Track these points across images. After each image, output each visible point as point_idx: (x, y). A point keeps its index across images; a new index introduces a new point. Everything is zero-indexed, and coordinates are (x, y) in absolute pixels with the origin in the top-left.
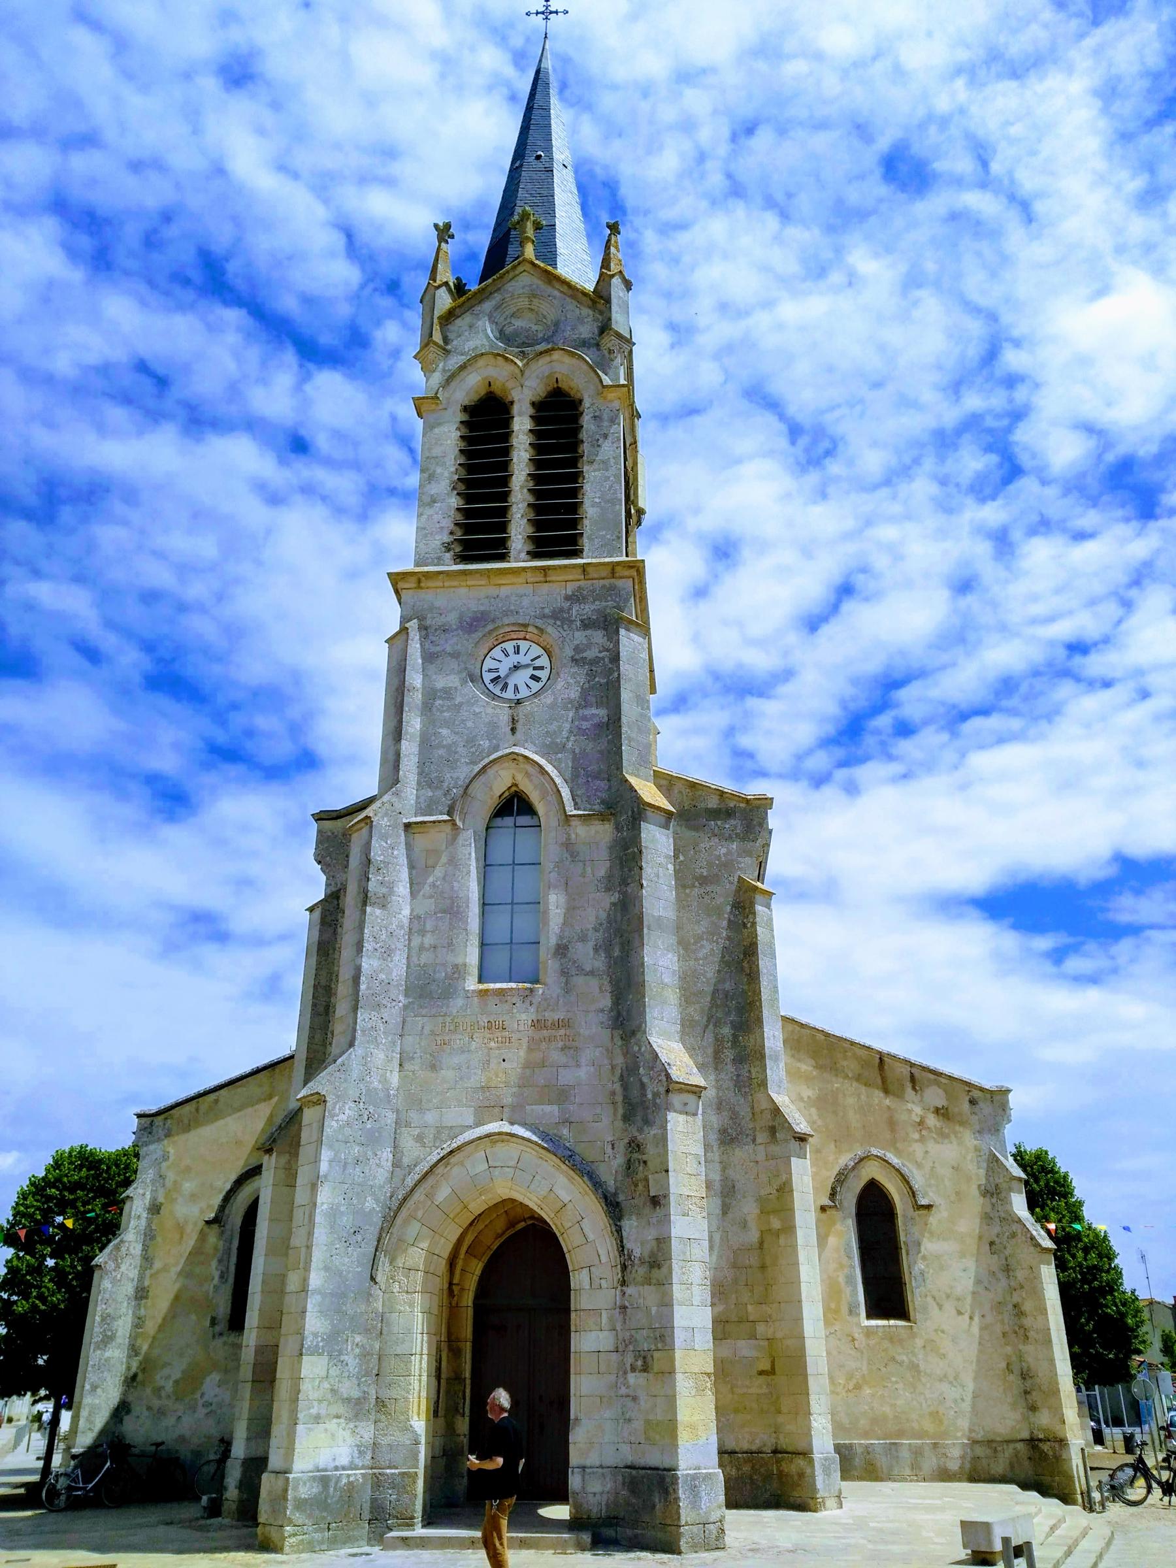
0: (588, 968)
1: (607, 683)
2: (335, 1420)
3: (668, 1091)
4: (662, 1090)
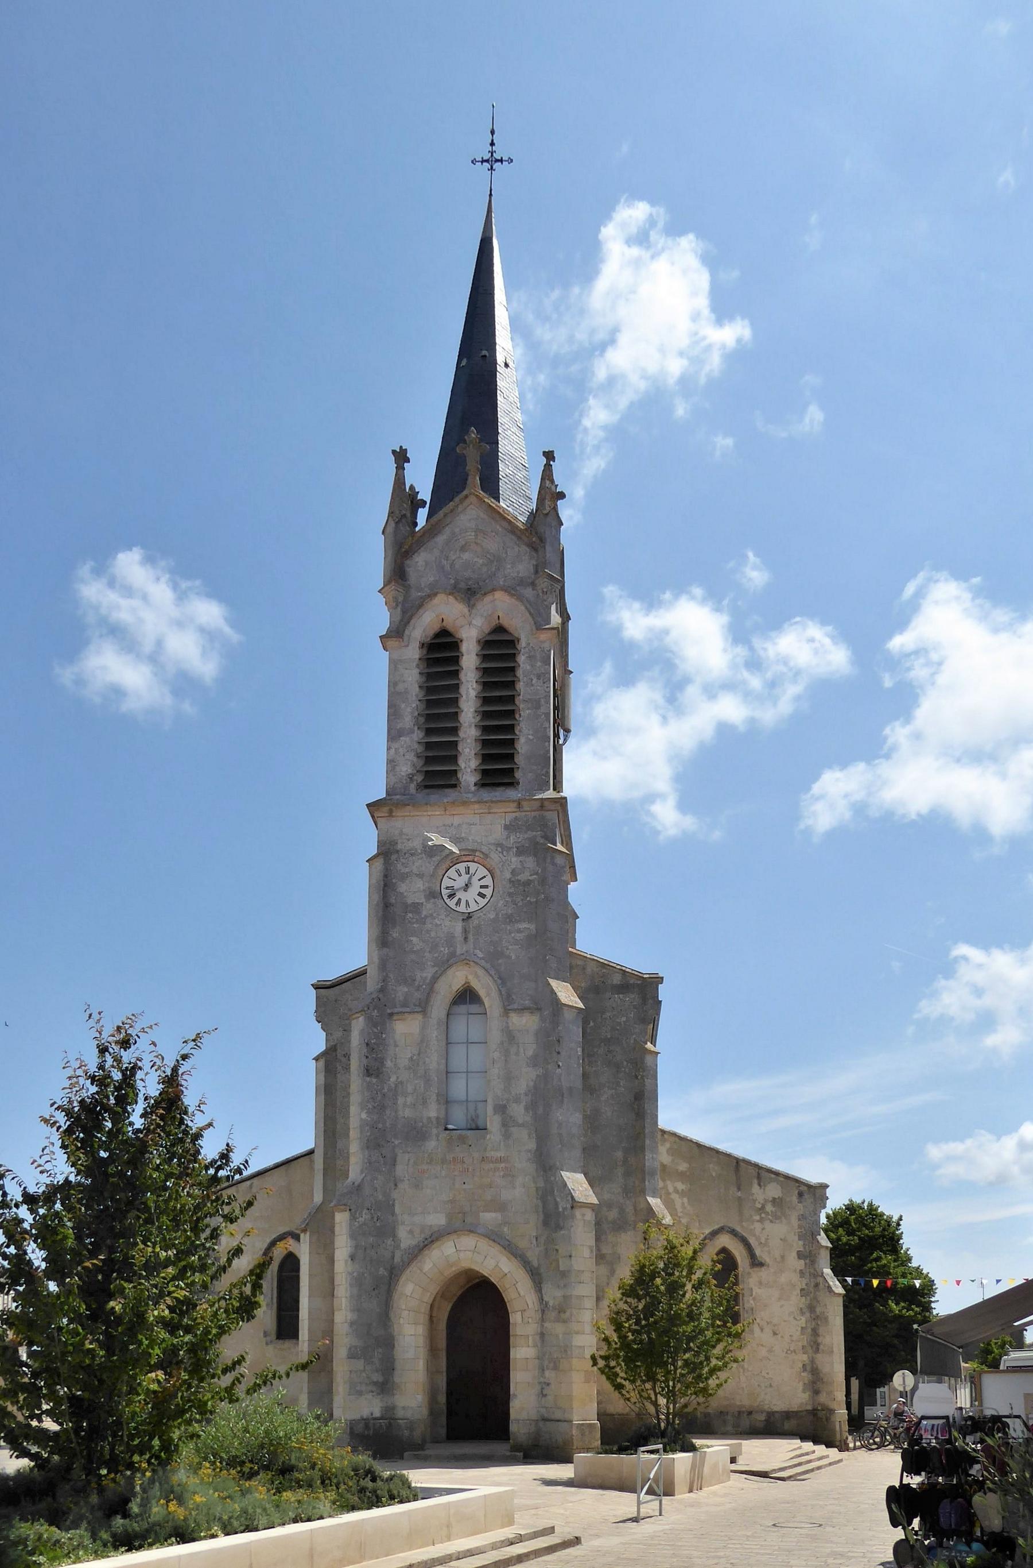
0: (520, 1121)
1: (536, 902)
3: (572, 1207)
4: (569, 1206)
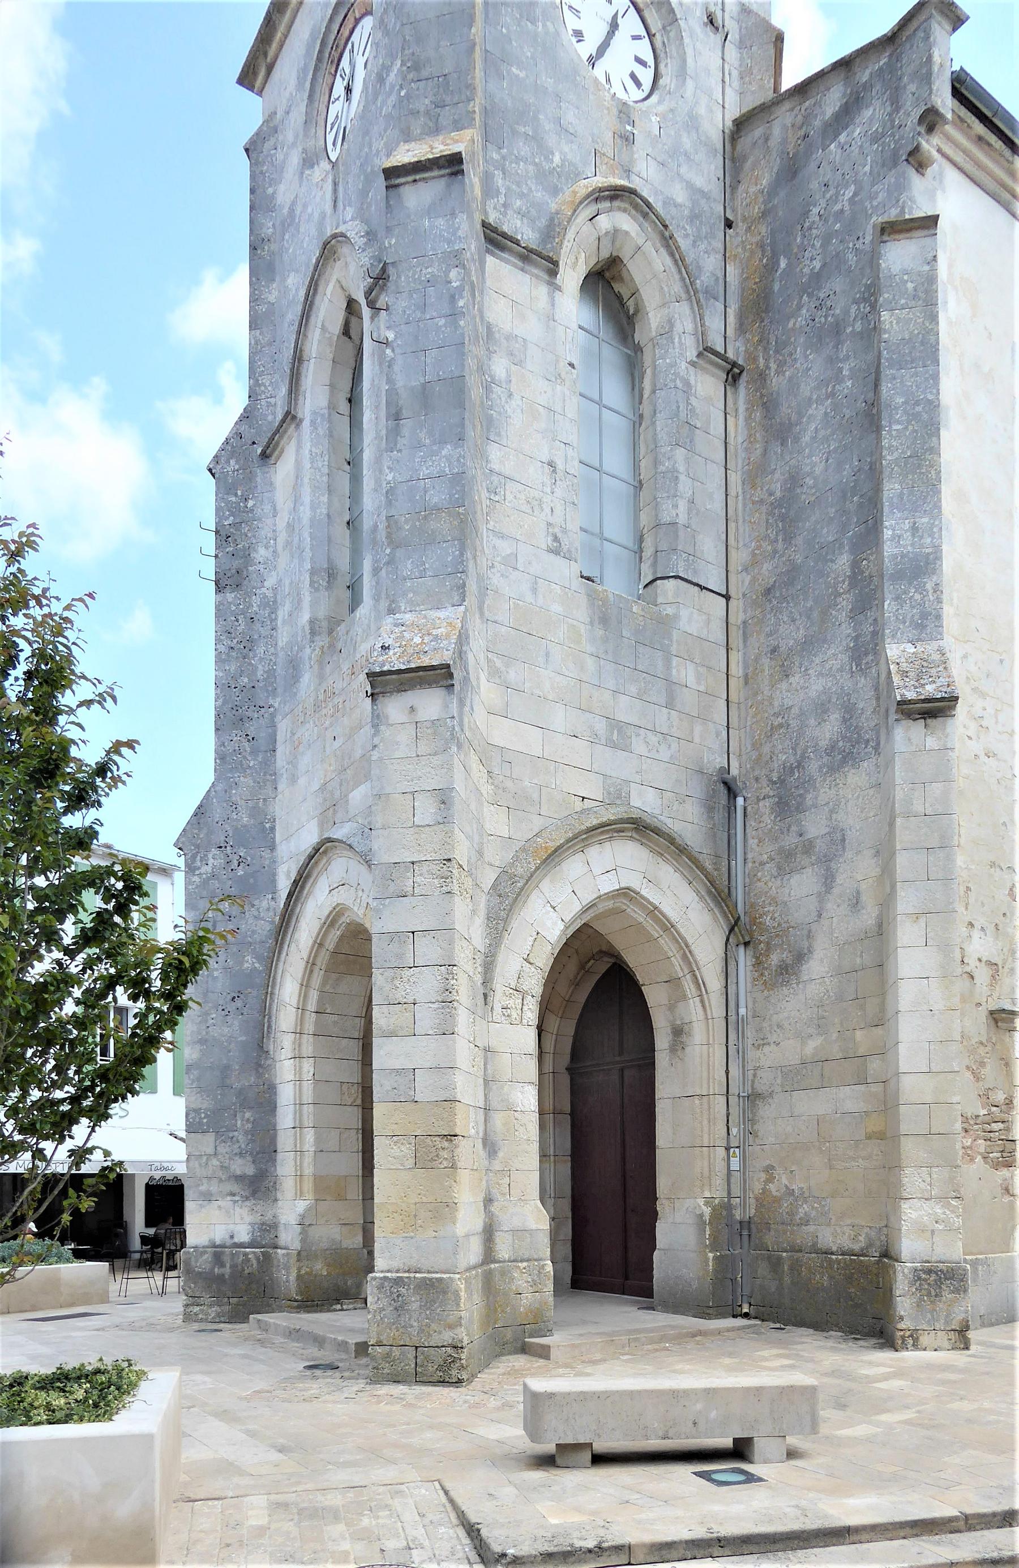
2: (229, 1198)
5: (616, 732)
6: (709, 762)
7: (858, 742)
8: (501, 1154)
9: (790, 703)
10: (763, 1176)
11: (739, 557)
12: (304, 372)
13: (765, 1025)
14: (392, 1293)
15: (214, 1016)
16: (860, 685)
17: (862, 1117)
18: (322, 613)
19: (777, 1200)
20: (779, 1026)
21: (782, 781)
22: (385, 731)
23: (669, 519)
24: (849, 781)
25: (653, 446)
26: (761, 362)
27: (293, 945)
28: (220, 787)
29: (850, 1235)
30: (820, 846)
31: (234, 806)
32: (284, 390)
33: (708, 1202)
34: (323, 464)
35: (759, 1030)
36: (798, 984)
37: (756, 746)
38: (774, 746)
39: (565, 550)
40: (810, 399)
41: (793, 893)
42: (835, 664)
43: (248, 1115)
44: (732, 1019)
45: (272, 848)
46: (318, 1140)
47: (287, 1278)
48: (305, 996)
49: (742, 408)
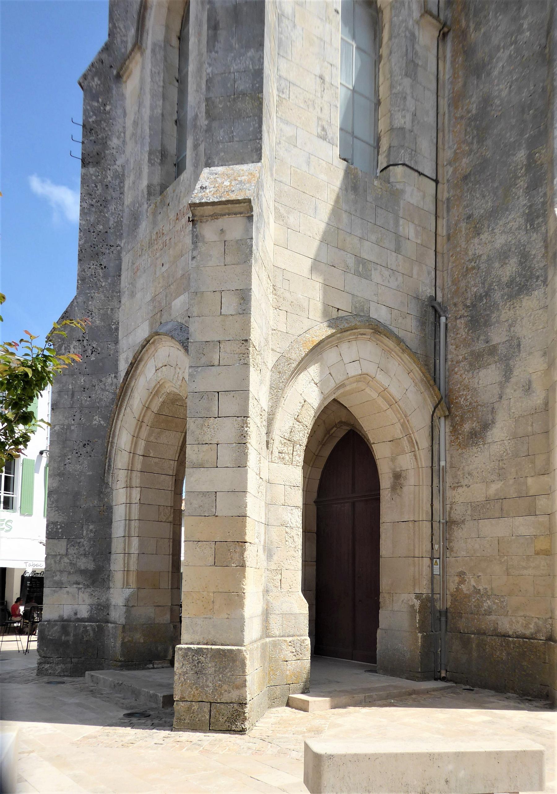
2: (75, 586)
5: (361, 265)
6: (423, 292)
7: (531, 278)
8: (275, 558)
9: (481, 253)
10: (457, 579)
11: (447, 154)
12: (147, 16)
13: (459, 473)
14: (193, 660)
15: (70, 457)
16: (532, 239)
17: (532, 538)
18: (157, 180)
19: (467, 597)
20: (469, 474)
21: (474, 306)
22: (202, 247)
23: (399, 126)
24: (524, 304)
25: (389, 76)
26: (464, 23)
27: (128, 409)
28: (80, 300)
29: (523, 623)
30: (502, 350)
31: (90, 313)
32: (132, 32)
33: (418, 596)
34: (160, 80)
35: (455, 476)
36: (484, 445)
37: (455, 282)
38: (468, 282)
39: (330, 137)
40: (499, 46)
41: (481, 382)
42: (515, 225)
43: (91, 527)
44: (436, 468)
45: (116, 342)
46: (141, 545)
47: (115, 644)
48: (136, 443)
49: (449, 55)
